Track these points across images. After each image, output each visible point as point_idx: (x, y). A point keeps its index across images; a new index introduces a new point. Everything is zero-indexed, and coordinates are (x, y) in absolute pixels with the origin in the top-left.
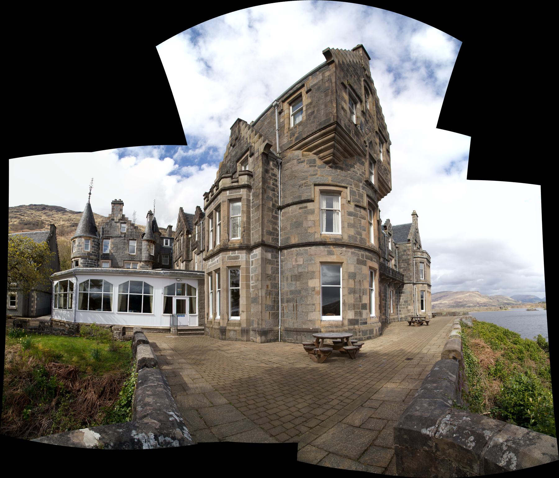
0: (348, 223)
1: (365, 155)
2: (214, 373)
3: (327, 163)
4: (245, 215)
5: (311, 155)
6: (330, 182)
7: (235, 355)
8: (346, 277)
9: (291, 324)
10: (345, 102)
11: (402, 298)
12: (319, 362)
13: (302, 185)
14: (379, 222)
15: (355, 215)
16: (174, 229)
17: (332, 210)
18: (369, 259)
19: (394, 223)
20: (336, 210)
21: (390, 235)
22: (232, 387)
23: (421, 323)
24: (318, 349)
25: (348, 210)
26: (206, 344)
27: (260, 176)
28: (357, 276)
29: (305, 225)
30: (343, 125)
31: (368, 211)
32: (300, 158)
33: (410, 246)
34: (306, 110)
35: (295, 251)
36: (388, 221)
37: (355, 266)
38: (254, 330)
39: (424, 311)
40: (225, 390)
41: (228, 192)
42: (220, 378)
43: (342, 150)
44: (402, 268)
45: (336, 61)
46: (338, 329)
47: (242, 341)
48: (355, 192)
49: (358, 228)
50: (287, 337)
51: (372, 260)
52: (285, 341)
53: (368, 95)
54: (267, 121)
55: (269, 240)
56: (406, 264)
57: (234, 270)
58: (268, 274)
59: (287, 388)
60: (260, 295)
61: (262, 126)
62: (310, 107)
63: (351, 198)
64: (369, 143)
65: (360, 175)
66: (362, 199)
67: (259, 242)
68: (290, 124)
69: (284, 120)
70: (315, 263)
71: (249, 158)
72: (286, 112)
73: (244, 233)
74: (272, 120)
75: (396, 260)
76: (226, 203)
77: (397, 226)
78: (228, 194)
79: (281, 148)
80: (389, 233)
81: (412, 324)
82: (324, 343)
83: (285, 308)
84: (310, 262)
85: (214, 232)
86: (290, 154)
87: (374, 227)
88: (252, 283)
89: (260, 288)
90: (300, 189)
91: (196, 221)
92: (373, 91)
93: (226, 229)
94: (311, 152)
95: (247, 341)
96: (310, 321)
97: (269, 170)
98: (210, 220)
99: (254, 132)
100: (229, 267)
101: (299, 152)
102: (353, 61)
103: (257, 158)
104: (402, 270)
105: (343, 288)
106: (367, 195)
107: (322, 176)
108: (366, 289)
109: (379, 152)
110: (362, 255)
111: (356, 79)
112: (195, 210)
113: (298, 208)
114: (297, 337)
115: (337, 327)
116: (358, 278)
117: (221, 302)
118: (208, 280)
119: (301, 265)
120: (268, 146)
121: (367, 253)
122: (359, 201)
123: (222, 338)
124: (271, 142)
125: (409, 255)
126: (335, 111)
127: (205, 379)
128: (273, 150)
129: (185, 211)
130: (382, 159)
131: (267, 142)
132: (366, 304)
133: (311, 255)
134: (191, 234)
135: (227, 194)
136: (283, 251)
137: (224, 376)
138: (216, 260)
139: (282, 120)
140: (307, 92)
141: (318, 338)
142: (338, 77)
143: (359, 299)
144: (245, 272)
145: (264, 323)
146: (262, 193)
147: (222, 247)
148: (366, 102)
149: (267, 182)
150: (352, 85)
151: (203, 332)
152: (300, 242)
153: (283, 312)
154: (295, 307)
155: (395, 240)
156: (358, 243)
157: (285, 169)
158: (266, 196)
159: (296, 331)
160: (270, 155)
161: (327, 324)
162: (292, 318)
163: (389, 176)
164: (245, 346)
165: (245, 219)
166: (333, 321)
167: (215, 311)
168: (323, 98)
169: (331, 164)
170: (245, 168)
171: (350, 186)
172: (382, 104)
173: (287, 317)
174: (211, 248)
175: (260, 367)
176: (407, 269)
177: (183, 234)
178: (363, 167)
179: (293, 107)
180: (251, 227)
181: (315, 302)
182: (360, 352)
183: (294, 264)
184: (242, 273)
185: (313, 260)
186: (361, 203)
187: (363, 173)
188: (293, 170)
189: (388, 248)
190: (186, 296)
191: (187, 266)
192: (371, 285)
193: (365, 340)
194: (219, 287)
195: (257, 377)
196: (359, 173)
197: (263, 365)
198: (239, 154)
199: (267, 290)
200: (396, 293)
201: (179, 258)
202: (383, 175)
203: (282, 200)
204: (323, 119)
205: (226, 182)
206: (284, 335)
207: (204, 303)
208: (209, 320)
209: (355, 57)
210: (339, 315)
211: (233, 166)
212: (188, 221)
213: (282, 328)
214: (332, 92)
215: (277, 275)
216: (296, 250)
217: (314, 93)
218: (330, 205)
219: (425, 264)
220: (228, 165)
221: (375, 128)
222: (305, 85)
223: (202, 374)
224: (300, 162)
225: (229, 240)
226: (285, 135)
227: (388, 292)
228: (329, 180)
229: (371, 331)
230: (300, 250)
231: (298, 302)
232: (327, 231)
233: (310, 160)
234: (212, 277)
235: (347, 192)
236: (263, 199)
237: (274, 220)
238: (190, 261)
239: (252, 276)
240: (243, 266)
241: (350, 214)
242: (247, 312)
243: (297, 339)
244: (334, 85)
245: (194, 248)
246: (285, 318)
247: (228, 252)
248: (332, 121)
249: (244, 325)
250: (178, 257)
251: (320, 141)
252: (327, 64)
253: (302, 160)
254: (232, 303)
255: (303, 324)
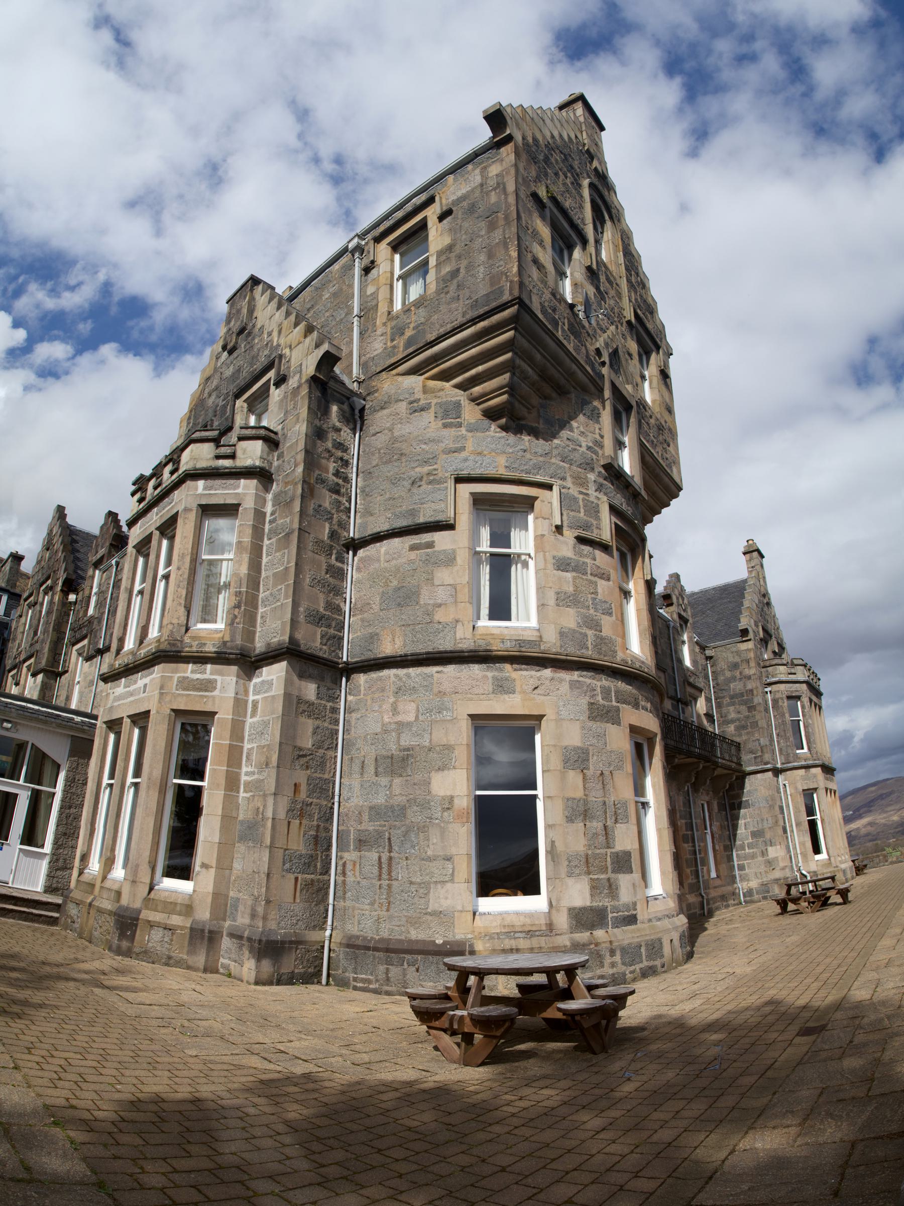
0: (558, 593)
1: (601, 390)
2: (63, 1062)
3: (491, 415)
4: (246, 558)
5: (448, 390)
7: (153, 1014)
8: (556, 762)
9: (369, 923)
10: (541, 243)
12: (467, 1062)
13: (421, 479)
14: (650, 585)
15: (579, 569)
16: (27, 566)
18: (629, 703)
20: (519, 555)
24: (465, 1013)
25: (556, 554)
27: (301, 445)
28: (593, 760)
30: (536, 307)
31: (615, 553)
32: (417, 396)
34: (438, 265)
35: (393, 679)
37: (583, 728)
38: (236, 936)
41: (201, 483)
42: (83, 1085)
43: (536, 377)
45: (518, 137)
46: (535, 942)
47: (189, 968)
48: (575, 499)
50: (350, 968)
51: (636, 706)
52: (343, 984)
53: (603, 223)
54: (331, 290)
57: (196, 725)
58: (300, 749)
59: (340, 1155)
60: (269, 814)
62: (448, 258)
63: (565, 518)
64: (610, 355)
65: (589, 448)
66: (598, 518)
67: (279, 643)
68: (391, 301)
69: (378, 289)
70: (454, 720)
71: (272, 388)
72: (382, 268)
73: (236, 611)
74: (344, 288)
76: (192, 516)
79: (363, 365)
82: (486, 992)
83: (349, 866)
84: (439, 717)
86: (388, 385)
87: (637, 602)
88: (247, 772)
89: (273, 790)
91: (98, 556)
92: (614, 211)
93: (184, 592)
94: (448, 381)
95: (205, 970)
96: (437, 914)
97: (327, 432)
98: (141, 560)
99: (292, 318)
100: (177, 712)
101: (415, 381)
102: (561, 136)
103: (296, 391)
106: (613, 509)
107: (480, 454)
108: (625, 804)
109: (639, 380)
110: (606, 692)
111: (568, 181)
112: (102, 521)
113: (407, 546)
114: (387, 971)
115: (530, 934)
116: (595, 765)
119: (409, 724)
120: (329, 360)
121: (621, 685)
122: (587, 527)
123: (119, 947)
124: (339, 348)
128: (343, 372)
129: (70, 520)
130: (648, 398)
131: (325, 347)
132: (628, 854)
133: (442, 694)
134: (76, 591)
135: (196, 489)
136: (354, 676)
137: (101, 1079)
139: (370, 290)
140: (441, 218)
141: (464, 974)
142: (523, 179)
143: (602, 839)
144: (228, 736)
145: (273, 914)
146: (303, 497)
147: (163, 647)
148: (598, 242)
150: (559, 198)
152: (410, 649)
153: (344, 882)
154: (385, 866)
156: (590, 653)
157: (372, 432)
158: (312, 506)
159: (388, 950)
160: (332, 384)
161: (495, 927)
163: (671, 449)
164: (198, 988)
165: (244, 570)
166: (517, 914)
167: (113, 850)
168: (483, 233)
170: (259, 418)
172: (639, 244)
173: (357, 899)
174: (130, 644)
175: (240, 1067)
177: (51, 588)
178: (597, 426)
179: (402, 256)
180: (261, 595)
181: (453, 851)
182: (620, 1024)
183: (386, 719)
184: (218, 738)
185: (447, 709)
186: (596, 531)
187: (596, 442)
188: (396, 434)
190: (21, 782)
191: (46, 690)
192: (639, 790)
193: (634, 980)
194: (137, 773)
195: (224, 1102)
196: (584, 444)
197: (255, 1062)
198: (245, 375)
199: (294, 802)
201: (25, 661)
202: (655, 447)
204: (483, 290)
206: (343, 962)
207: (78, 817)
209: (565, 125)
210: (536, 891)
211: (224, 407)
212: (74, 551)
213: (338, 937)
214: (506, 218)
216: (396, 676)
217: (459, 221)
218: (501, 538)
220: (210, 402)
221: (625, 313)
222: (437, 199)
223: (18, 1056)
224: (417, 409)
226: (379, 332)
228: (499, 466)
229: (654, 948)
230: (408, 676)
231: (395, 848)
233: (446, 403)
234: (118, 735)
236: (303, 513)
237: (331, 580)
240: (225, 714)
241: (563, 565)
242: (219, 868)
243: (388, 979)
244: (512, 199)
245: (78, 636)
246: (348, 903)
247: (182, 666)
248: (506, 297)
249: (203, 914)
250: (22, 657)
251: (473, 351)
252: (496, 145)
253: (422, 402)
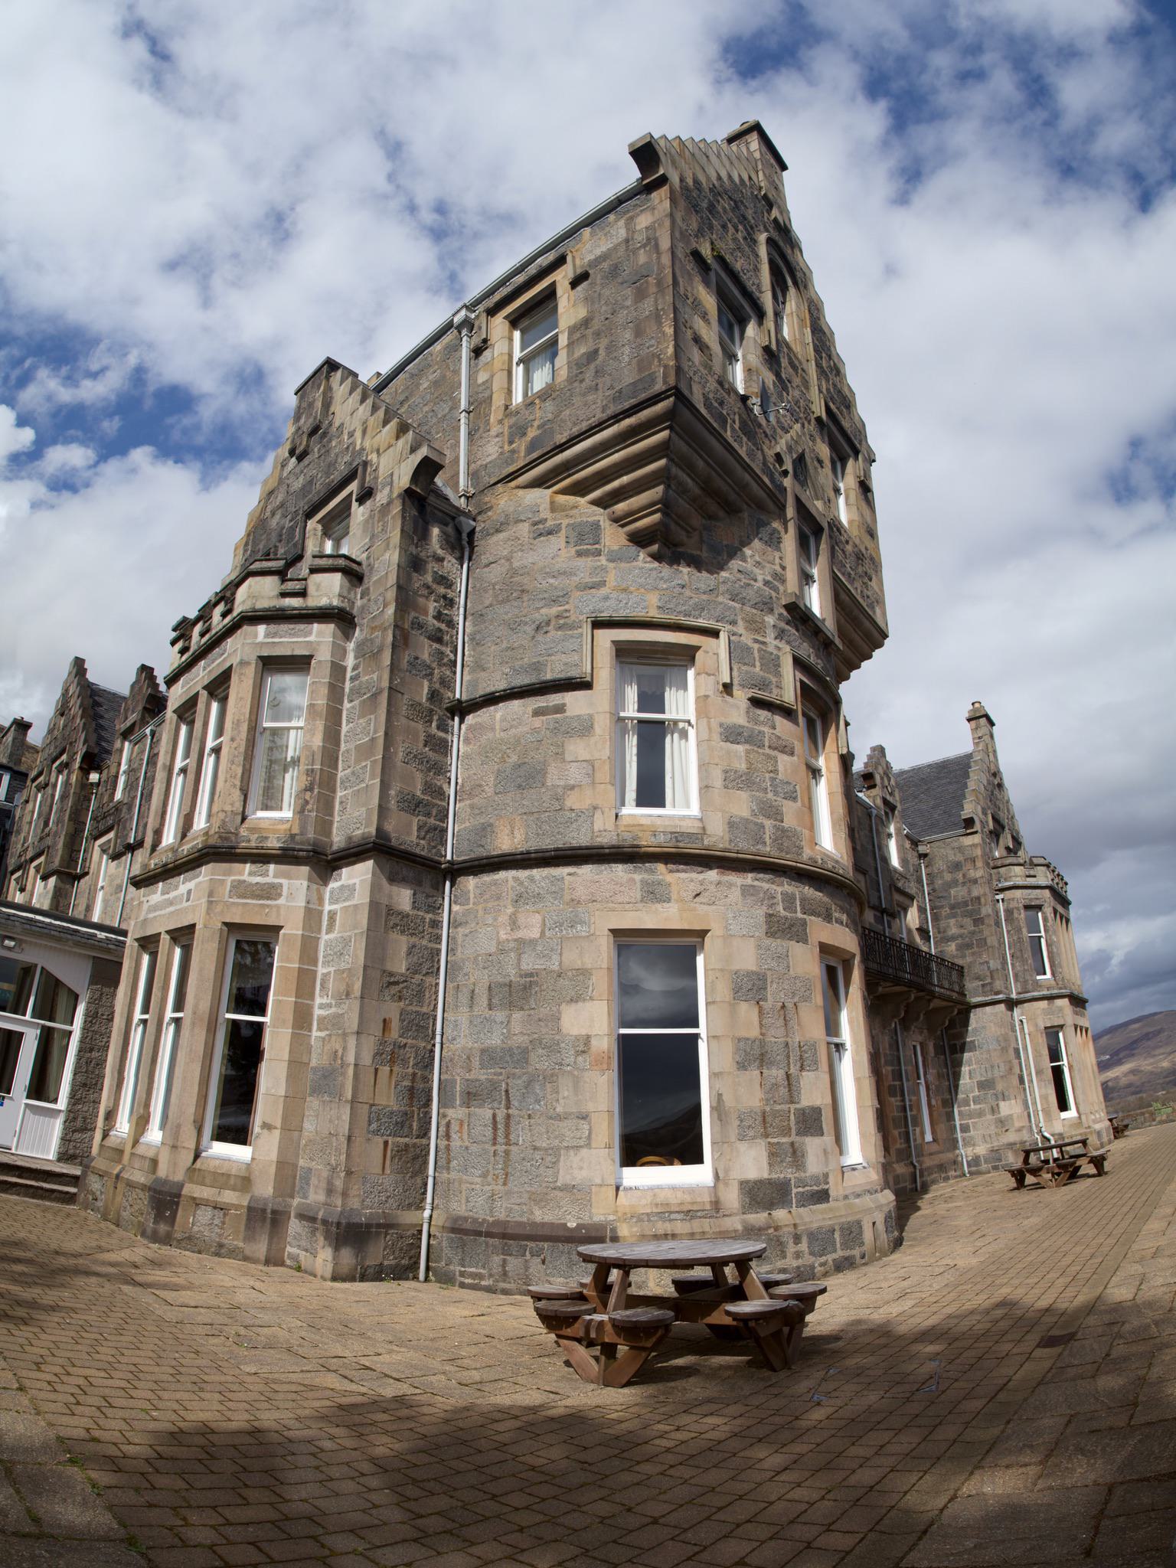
1: (782, 508)
3: (639, 539)
4: (320, 725)
5: (583, 507)
6: (654, 614)
7: (199, 1319)
8: (724, 992)
9: (481, 1201)
10: (704, 316)
11: (965, 1069)
13: (548, 623)
14: (846, 760)
16: (36, 737)
17: (662, 723)
18: (818, 915)
19: (901, 760)
20: (676, 722)
21: (890, 807)
22: (159, 1464)
23: (1068, 1171)
24: (605, 1317)
25: (723, 720)
26: (74, 1245)
27: (392, 579)
28: (771, 989)
29: (553, 777)
31: (801, 719)
32: (543, 515)
33: (974, 846)
34: (570, 345)
35: (511, 883)
36: (880, 751)
37: (759, 947)
39: (1071, 1114)
40: (120, 1470)
41: (261, 629)
42: (109, 1412)
43: (697, 491)
44: (953, 938)
45: (674, 178)
47: (246, 1259)
48: (749, 649)
49: (765, 790)
50: (456, 1259)
51: (828, 918)
53: (785, 290)
54: (431, 378)
55: (407, 833)
56: (968, 921)
57: (254, 944)
58: (391, 974)
60: (351, 1058)
61: (411, 394)
62: (583, 336)
63: (735, 673)
64: (794, 462)
65: (766, 583)
66: (778, 674)
67: (364, 837)
68: (509, 392)
70: (590, 937)
71: (355, 504)
72: (498, 348)
73: (308, 794)
75: (922, 910)
76: (250, 672)
77: (913, 770)
78: (261, 638)
79: (473, 475)
80: (885, 801)
81: (1030, 1179)
82: (633, 1291)
83: (454, 1127)
84: (571, 933)
85: (191, 775)
86: (504, 501)
87: (829, 782)
88: (321, 1005)
90: (540, 638)
91: (128, 723)
92: (799, 275)
93: (239, 771)
94: (583, 496)
98: (184, 729)
99: (381, 413)
101: (540, 497)
102: (730, 177)
103: (385, 509)
104: (951, 948)
105: (711, 1038)
107: (625, 590)
109: (832, 494)
110: (789, 900)
111: (740, 236)
113: (530, 710)
115: (689, 1214)
116: (774, 996)
117: (178, 1071)
118: (136, 967)
119: (532, 942)
120: (428, 469)
121: (809, 891)
122: (764, 685)
123: (155, 1232)
125: (975, 881)
126: (671, 350)
127: (32, 1400)
128: (446, 483)
129: (91, 677)
130: (844, 517)
131: (424, 451)
133: (575, 902)
134: (98, 769)
135: (256, 636)
137: (131, 1403)
138: (183, 889)
139: (482, 377)
140: (575, 284)
141: (604, 1266)
142: (681, 233)
144: (297, 958)
145: (356, 1190)
146: (394, 646)
147: (212, 841)
149: (416, 607)
150: (728, 258)
151: (73, 1190)
152: (534, 845)
153: (448, 1148)
154: (501, 1127)
155: (910, 826)
156: (768, 850)
157: (485, 561)
159: (504, 1236)
160: (432, 499)
161: (644, 1206)
162: (484, 1176)
163: (874, 584)
164: (258, 1285)
165: (318, 741)
166: (674, 1188)
167: (147, 1105)
168: (628, 303)
169: (655, 547)
170: (337, 544)
171: (728, 627)
172: (833, 317)
173: (465, 1169)
174: (169, 838)
175: (312, 1388)
176: (973, 943)
177: (66, 765)
178: (777, 554)
180: (340, 775)
181: (590, 1107)
183: (503, 936)
184: (283, 960)
185: (582, 923)
186: (775, 691)
187: (775, 575)
189: (885, 860)
190: (28, 1017)
191: (59, 896)
196: (760, 578)
197: (332, 1381)
198: (319, 488)
200: (937, 1054)
201: (32, 860)
202: (852, 581)
203: (465, 678)
204: (629, 377)
205: (260, 592)
206: (447, 1252)
207: (101, 1063)
208: (111, 1141)
209: (736, 162)
210: (698, 1159)
211: (292, 529)
212: (97, 717)
213: (439, 1219)
214: (659, 283)
215: (429, 980)
216: (516, 879)
217: (598, 288)
218: (651, 700)
219: (1048, 911)
220: (274, 523)
221: (814, 408)
222: (569, 258)
223: (24, 1373)
224: (543, 532)
225: (244, 819)
227: (905, 1053)
228: (650, 606)
230: (532, 879)
231: (515, 1103)
232: (641, 802)
233: (580, 524)
235: (716, 652)
236: (394, 667)
238: (79, 877)
239: (325, 975)
240: (292, 930)
241: (732, 735)
242: (286, 1129)
243: (505, 1274)
244: (666, 260)
245: (102, 827)
246: (453, 1175)
247: (237, 866)
248: (659, 386)
249: (265, 1189)
250: (30, 854)
253: (549, 523)
254: (227, 1083)
255: (537, 1202)
